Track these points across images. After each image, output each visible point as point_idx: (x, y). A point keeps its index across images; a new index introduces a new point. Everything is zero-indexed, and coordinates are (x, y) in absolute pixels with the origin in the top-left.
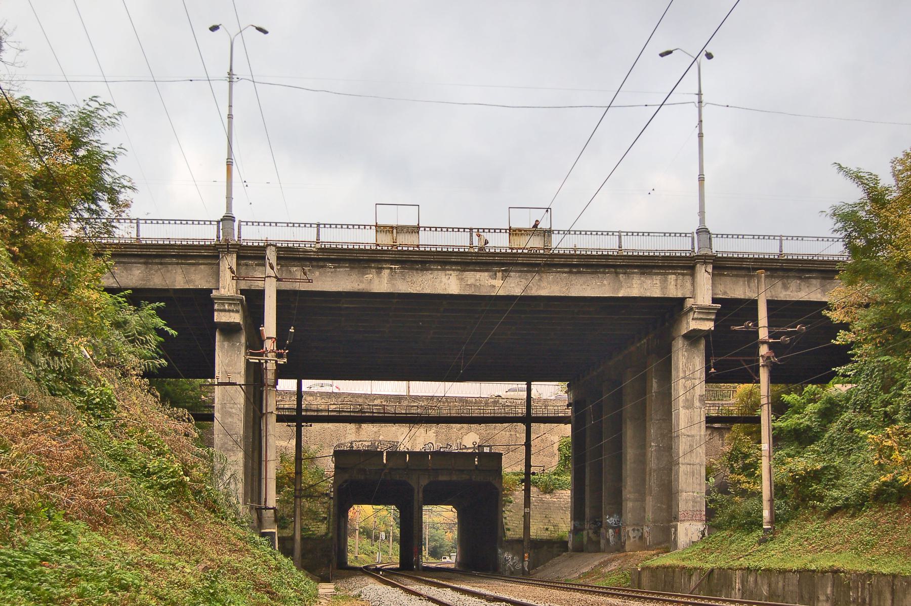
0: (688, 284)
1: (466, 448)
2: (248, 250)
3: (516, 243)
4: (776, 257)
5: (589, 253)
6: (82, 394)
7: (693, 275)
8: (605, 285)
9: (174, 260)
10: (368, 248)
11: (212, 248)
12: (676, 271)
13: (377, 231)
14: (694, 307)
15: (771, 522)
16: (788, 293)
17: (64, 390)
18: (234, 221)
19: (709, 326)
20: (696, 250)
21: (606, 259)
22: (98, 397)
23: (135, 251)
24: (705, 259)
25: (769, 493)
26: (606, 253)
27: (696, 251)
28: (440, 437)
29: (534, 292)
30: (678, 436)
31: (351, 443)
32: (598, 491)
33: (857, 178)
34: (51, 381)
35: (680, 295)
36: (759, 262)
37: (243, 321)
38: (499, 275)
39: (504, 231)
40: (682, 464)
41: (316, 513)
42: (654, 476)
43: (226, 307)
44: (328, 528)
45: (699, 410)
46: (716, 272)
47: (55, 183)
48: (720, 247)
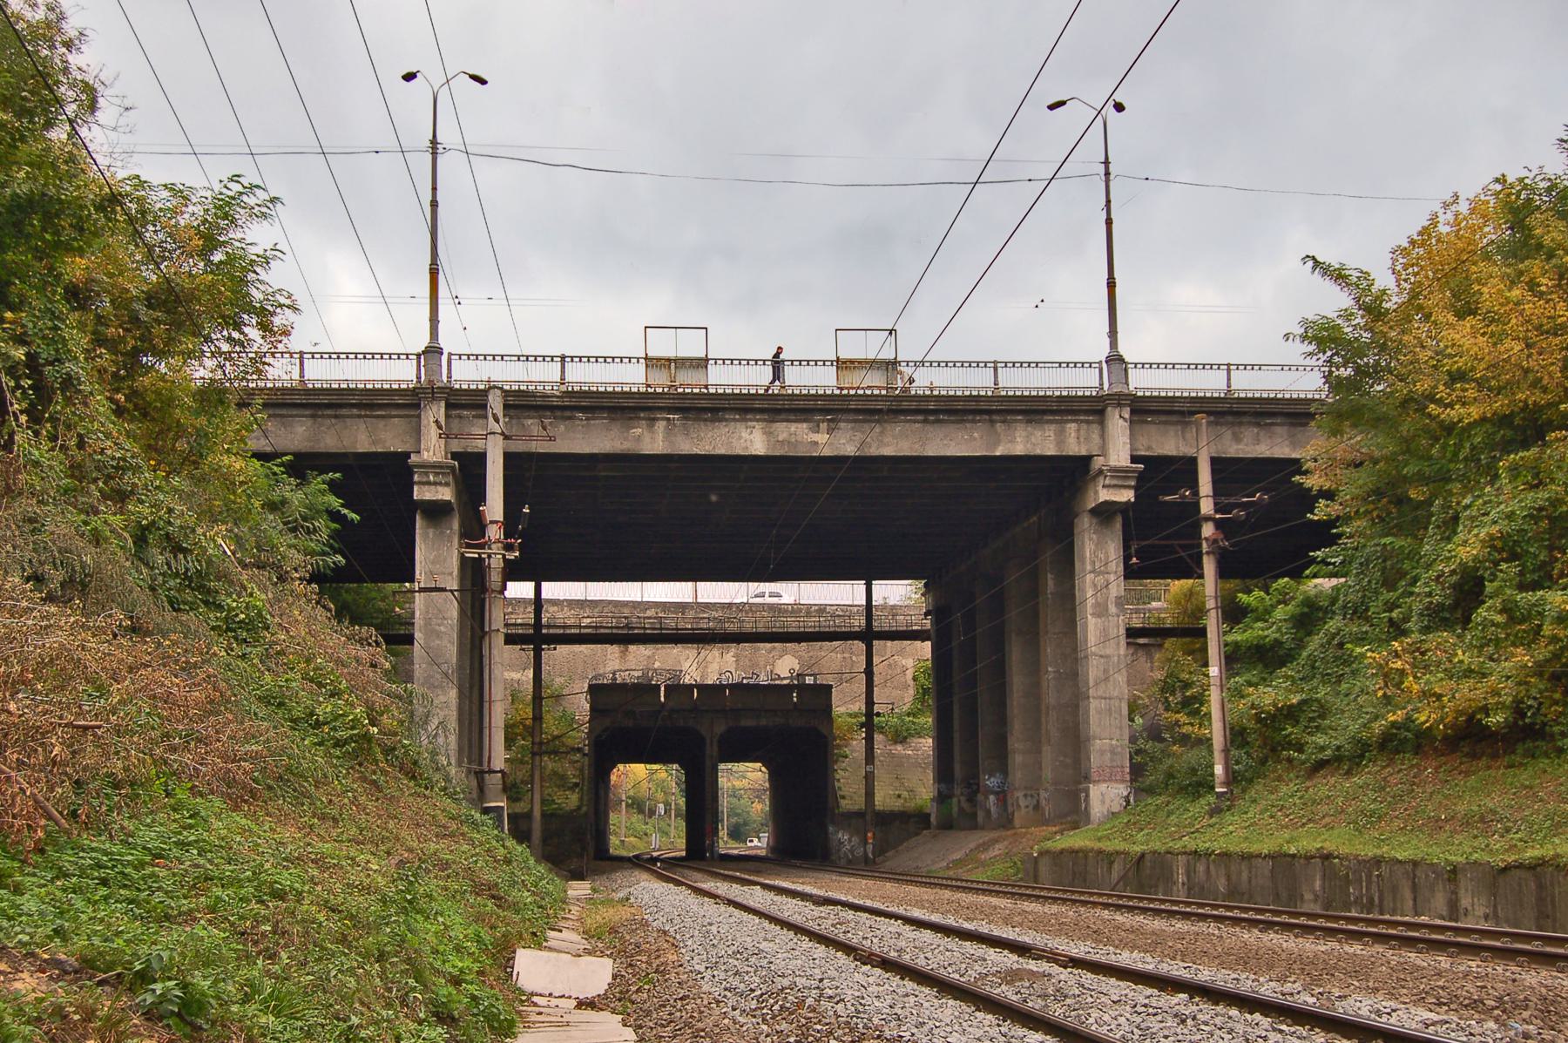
0: (1095, 437)
1: (780, 678)
4: (1222, 395)
6: (220, 607)
7: (1102, 423)
8: (975, 439)
9: (355, 411)
10: (634, 390)
13: (647, 366)
15: (1227, 783)
18: (442, 354)
19: (1127, 496)
20: (1106, 386)
22: (242, 612)
23: (297, 399)
24: (1119, 399)
29: (874, 450)
31: (614, 674)
33: (1338, 276)
35: (1084, 452)
38: (824, 426)
41: (563, 777)
43: (431, 478)
44: (581, 799)
45: (1116, 618)
46: (1135, 419)
48: (1141, 382)
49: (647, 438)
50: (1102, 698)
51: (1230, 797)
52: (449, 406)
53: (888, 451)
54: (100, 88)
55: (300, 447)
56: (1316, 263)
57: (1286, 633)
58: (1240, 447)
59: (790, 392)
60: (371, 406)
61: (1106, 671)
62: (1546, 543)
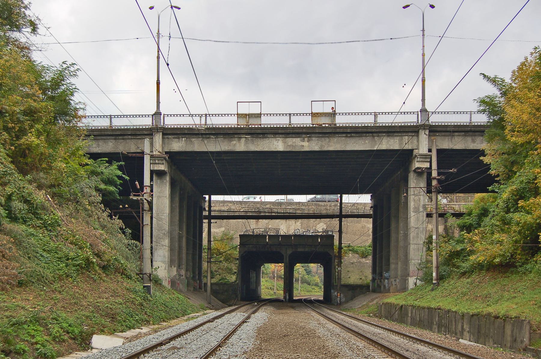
0: (415, 141)
1: (318, 232)
2: (168, 130)
3: (315, 121)
4: (468, 124)
5: (357, 125)
6: (42, 219)
7: (418, 136)
8: (366, 143)
9: (130, 137)
10: (233, 126)
11: (149, 130)
12: (408, 134)
13: (238, 117)
14: (417, 154)
15: (437, 279)
16: (475, 145)
17: (31, 218)
18: (161, 115)
20: (420, 122)
21: (366, 128)
22: (50, 221)
23: (109, 133)
24: (424, 127)
25: (436, 263)
26: (367, 125)
27: (419, 122)
28: (303, 226)
29: (326, 148)
30: (410, 228)
31: (253, 230)
32: (381, 258)
33: (494, 81)
34: (23, 214)
35: (410, 148)
36: (457, 127)
37: (168, 168)
38: (306, 139)
39: (308, 114)
40: (412, 244)
41: (231, 270)
42: (402, 250)
43: (157, 162)
44: (237, 278)
45: (422, 213)
46: (432, 134)
47: (35, 113)
48: (434, 119)
49: (238, 145)
50: (415, 244)
51: (438, 284)
52: (164, 134)
53: (331, 149)
54: (37, 22)
55: (111, 151)
56: (485, 76)
57: (475, 221)
58: (475, 145)
59: (293, 126)
60: (136, 135)
61: (418, 234)
62: (533, 193)
